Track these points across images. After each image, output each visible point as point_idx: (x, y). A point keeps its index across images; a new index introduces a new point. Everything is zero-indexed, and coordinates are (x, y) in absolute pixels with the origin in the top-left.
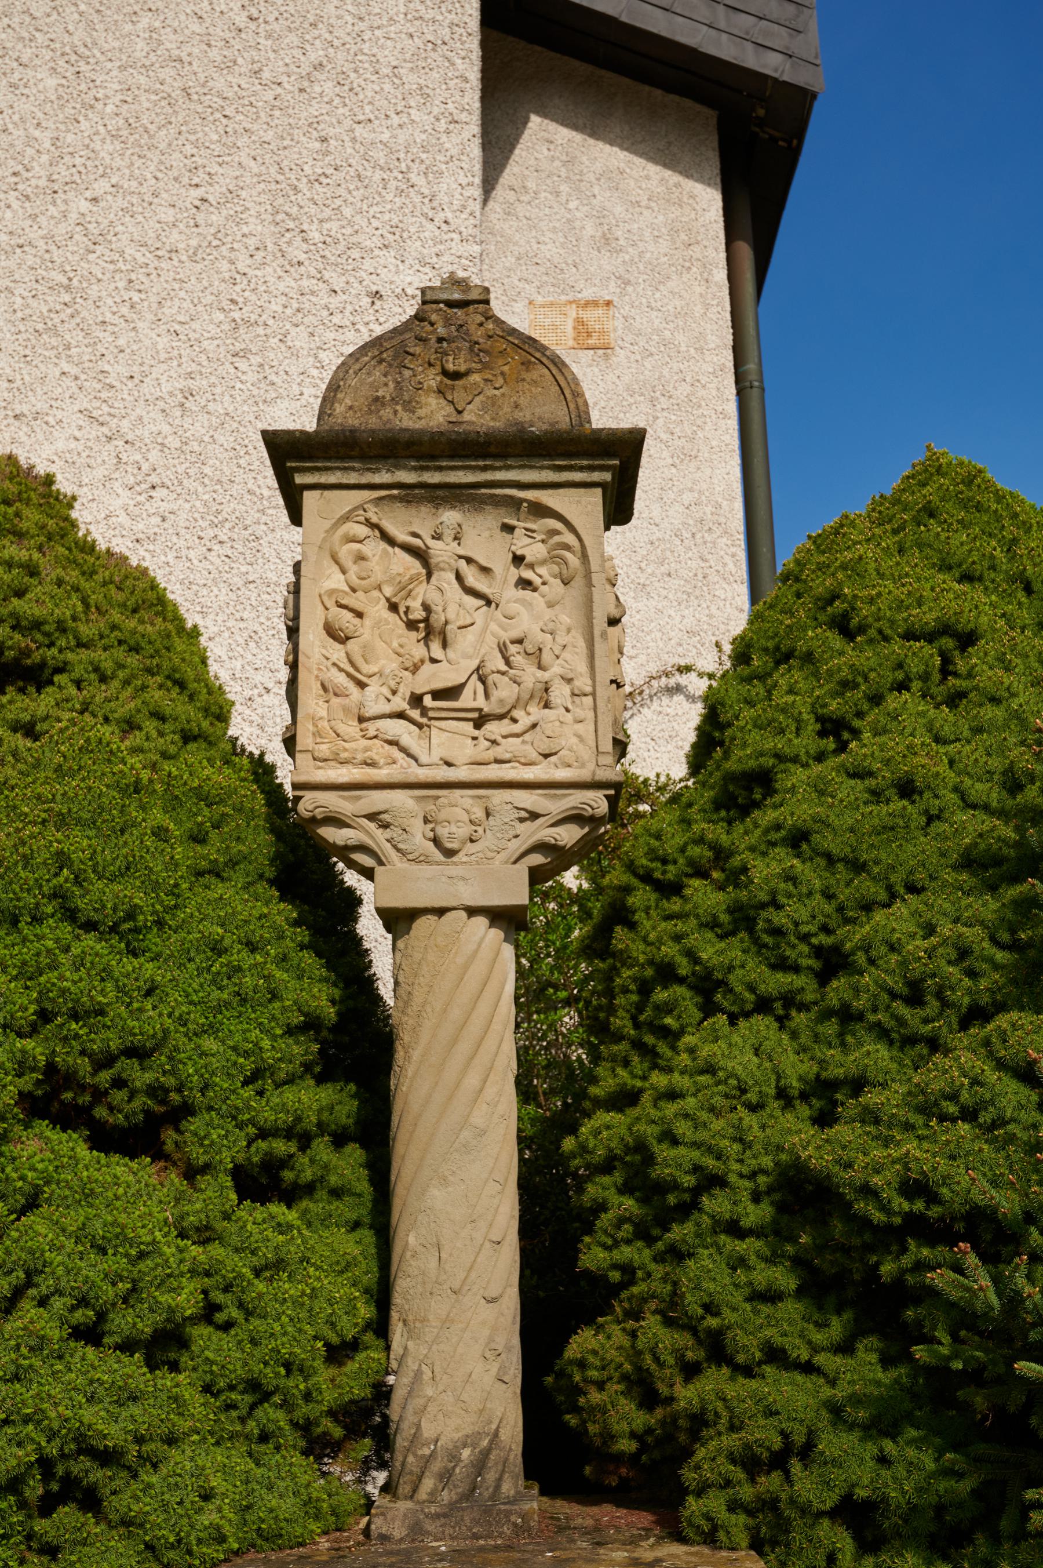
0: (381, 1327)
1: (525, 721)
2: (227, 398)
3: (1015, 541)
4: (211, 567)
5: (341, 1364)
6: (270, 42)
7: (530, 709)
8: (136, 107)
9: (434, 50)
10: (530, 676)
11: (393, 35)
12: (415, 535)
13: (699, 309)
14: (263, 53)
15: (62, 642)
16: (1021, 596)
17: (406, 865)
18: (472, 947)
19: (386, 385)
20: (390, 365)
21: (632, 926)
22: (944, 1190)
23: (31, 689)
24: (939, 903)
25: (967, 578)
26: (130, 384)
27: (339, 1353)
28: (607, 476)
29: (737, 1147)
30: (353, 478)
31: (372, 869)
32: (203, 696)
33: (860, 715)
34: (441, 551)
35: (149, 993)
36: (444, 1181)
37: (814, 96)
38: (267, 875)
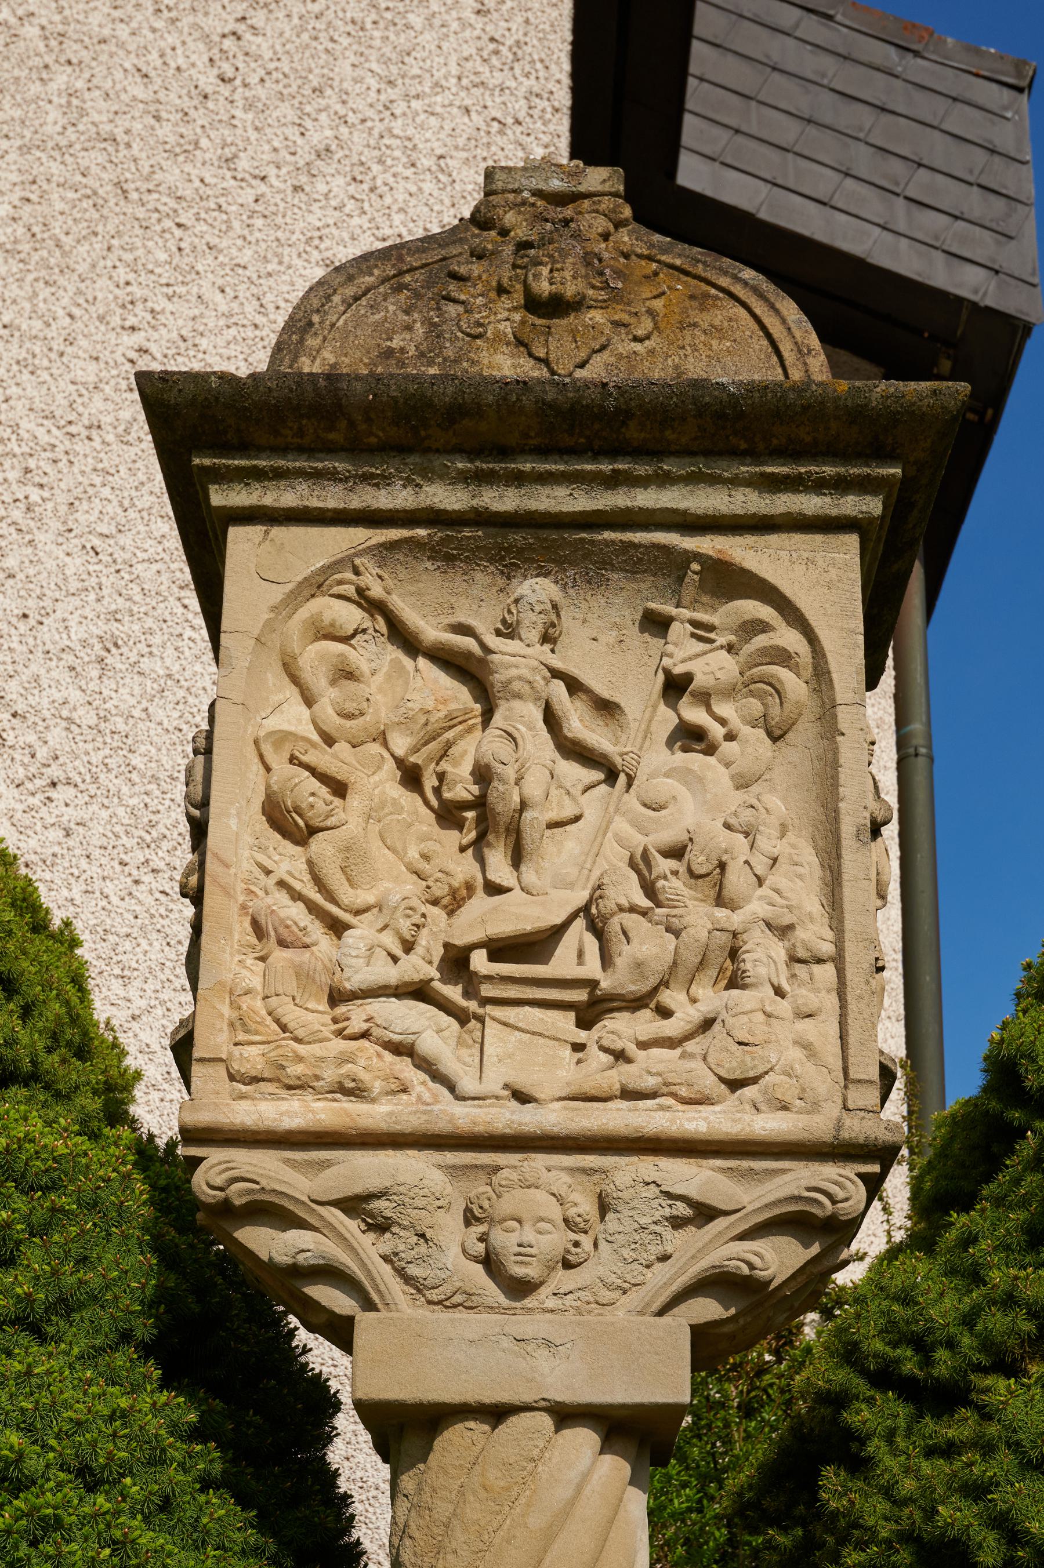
2: (170, 651)
4: (138, 908)
6: (250, 116)
7: (697, 990)
8: (44, 208)
9: (501, 132)
10: (700, 918)
11: (438, 109)
14: (239, 131)
17: (424, 1313)
18: (564, 1493)
19: (409, 328)
20: (418, 296)
21: (858, 1465)
26: (23, 627)
28: (873, 506)
30: (332, 497)
31: (350, 1320)
34: (516, 660)
38: (139, 1333)
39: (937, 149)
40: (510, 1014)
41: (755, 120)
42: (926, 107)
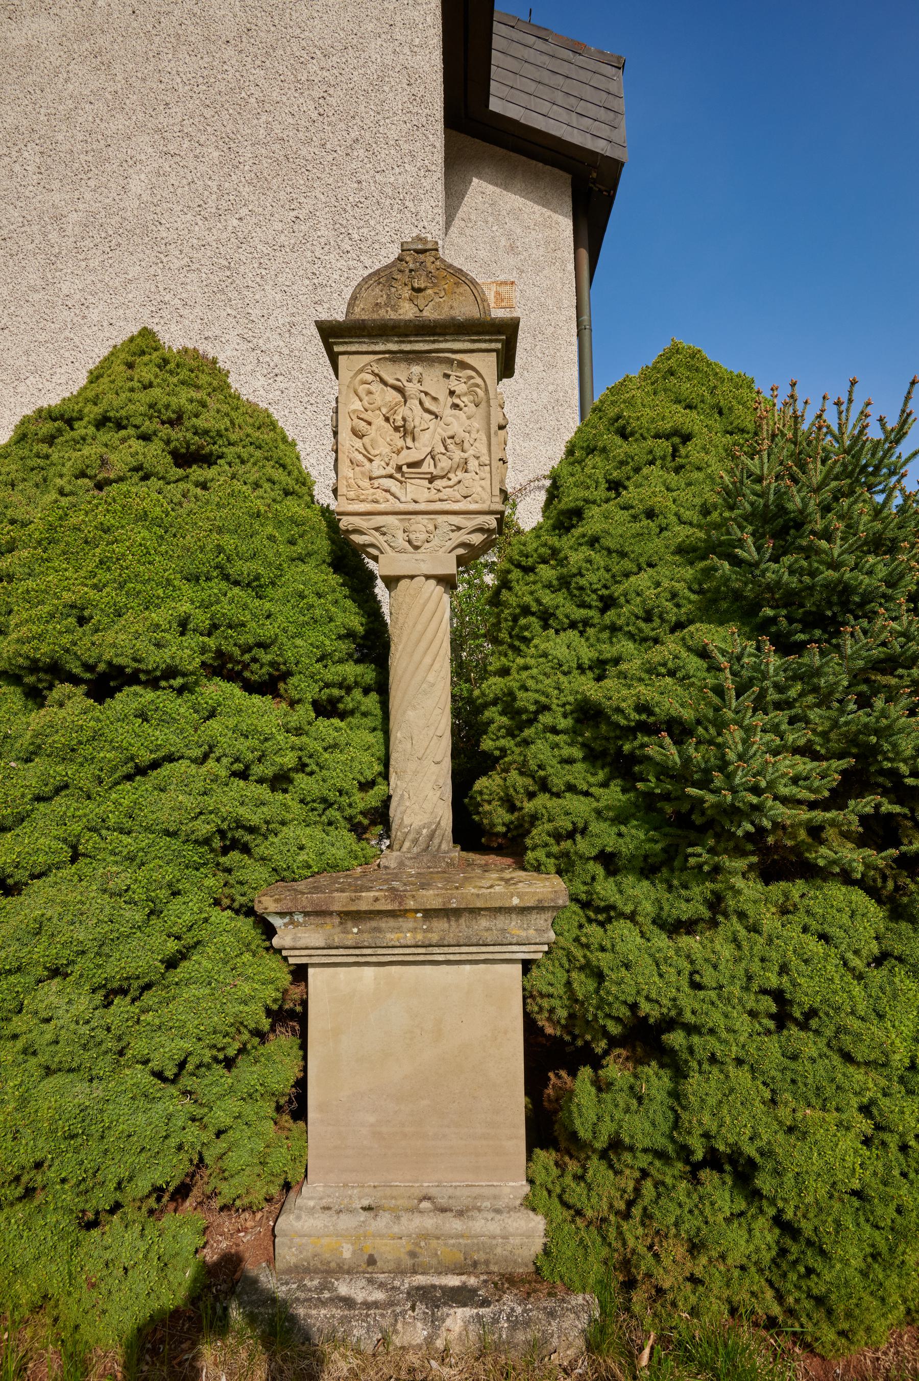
0: (385, 776)
1: (455, 479)
3: (715, 387)
5: (367, 792)
10: (457, 455)
12: (398, 380)
13: (559, 286)
15: (220, 442)
16: (716, 416)
18: (428, 595)
21: (510, 589)
22: (657, 709)
23: (205, 466)
24: (663, 572)
25: (689, 407)
27: (365, 786)
28: (499, 346)
29: (556, 692)
30: (364, 348)
32: (296, 473)
33: (628, 478)
34: (412, 388)
35: (268, 617)
36: (414, 708)
37: (623, 164)
39: (588, 93)
40: (412, 481)
41: (519, 82)
42: (584, 76)
